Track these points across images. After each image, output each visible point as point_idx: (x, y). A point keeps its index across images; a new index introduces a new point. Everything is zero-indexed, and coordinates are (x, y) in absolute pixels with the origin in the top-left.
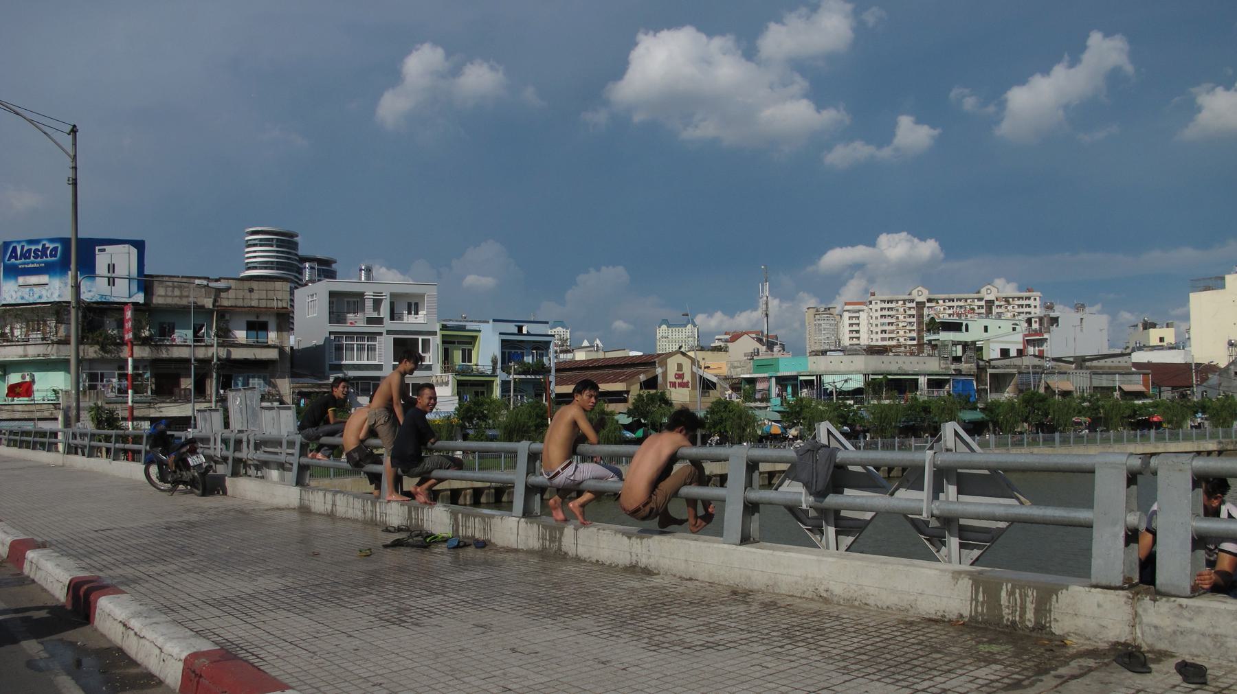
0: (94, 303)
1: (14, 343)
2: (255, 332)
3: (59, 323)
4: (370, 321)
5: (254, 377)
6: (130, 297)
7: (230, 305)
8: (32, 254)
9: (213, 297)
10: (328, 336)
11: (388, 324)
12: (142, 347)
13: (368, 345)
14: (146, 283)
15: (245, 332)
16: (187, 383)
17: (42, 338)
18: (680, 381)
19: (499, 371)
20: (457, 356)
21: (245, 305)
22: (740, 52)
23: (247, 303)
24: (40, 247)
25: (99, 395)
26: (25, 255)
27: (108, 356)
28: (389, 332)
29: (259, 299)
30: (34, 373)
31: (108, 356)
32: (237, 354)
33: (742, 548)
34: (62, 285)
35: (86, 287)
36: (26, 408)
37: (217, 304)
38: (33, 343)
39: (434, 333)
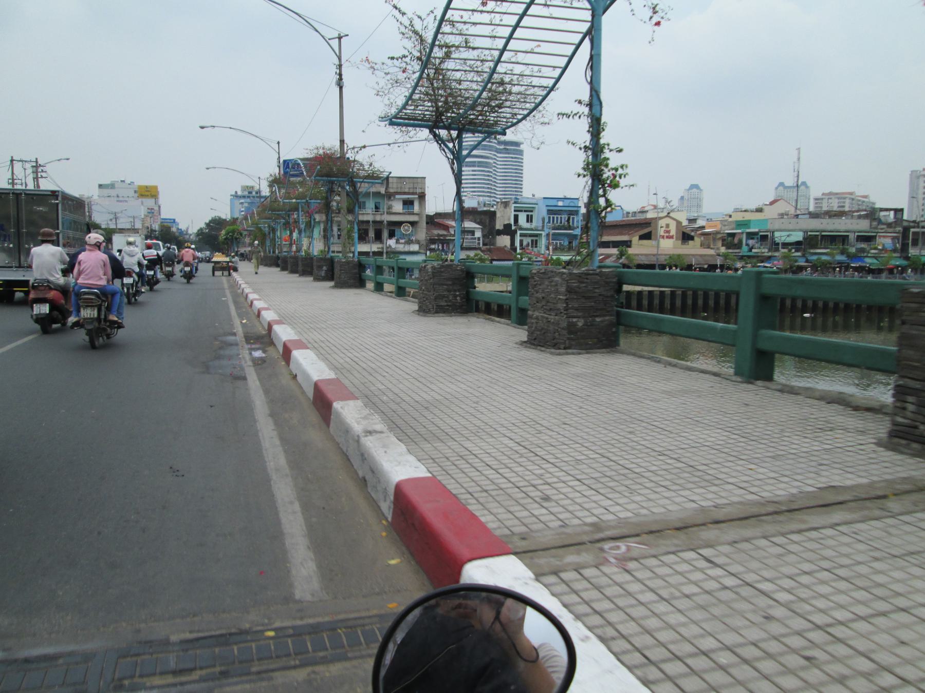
18: (667, 234)
19: (545, 229)
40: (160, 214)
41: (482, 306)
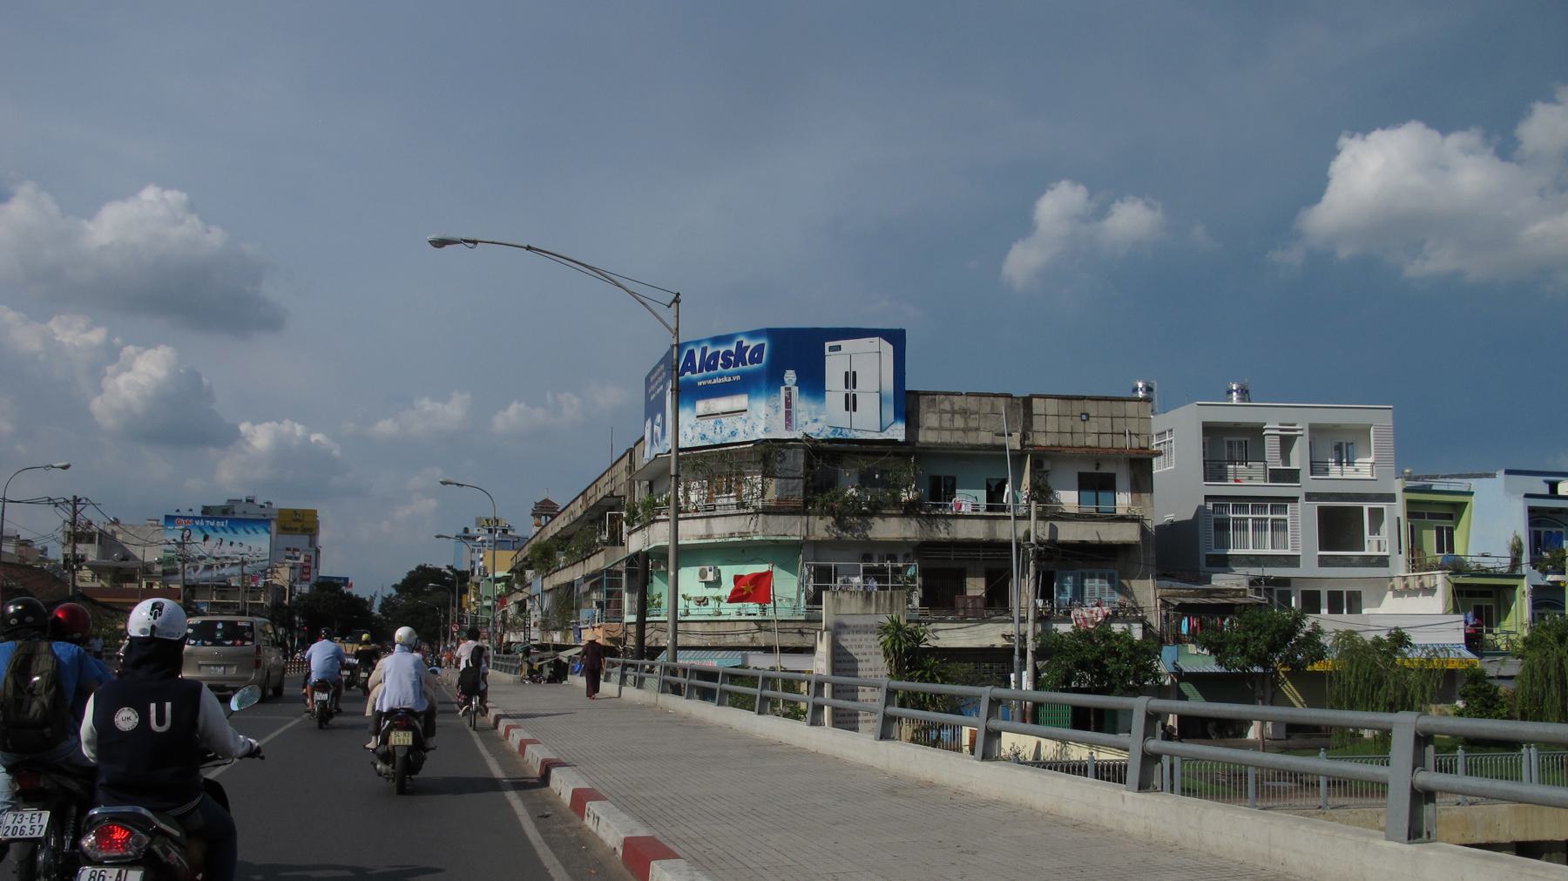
0: (824, 441)
1: (690, 515)
2: (1094, 494)
3: (766, 477)
4: (1276, 476)
5: (1092, 576)
6: (882, 430)
7: (1048, 444)
8: (720, 361)
9: (1020, 431)
10: (1203, 504)
11: (1308, 482)
12: (906, 520)
13: (1273, 520)
14: (907, 404)
15: (1077, 492)
16: (976, 587)
17: (737, 504)
19: (1525, 568)
20: (1430, 538)
21: (1075, 445)
22: (1491, 150)
23: (1078, 441)
24: (733, 348)
25: (895, 601)
26: (709, 364)
27: (847, 535)
28: (1310, 497)
29: (1099, 434)
30: (719, 567)
31: (847, 535)
32: (1070, 533)
33: (881, 742)
34: (772, 411)
35: (810, 413)
36: (709, 628)
37: (1027, 442)
38: (722, 513)
39: (1390, 498)
40: (317, 567)
41: (1210, 728)
